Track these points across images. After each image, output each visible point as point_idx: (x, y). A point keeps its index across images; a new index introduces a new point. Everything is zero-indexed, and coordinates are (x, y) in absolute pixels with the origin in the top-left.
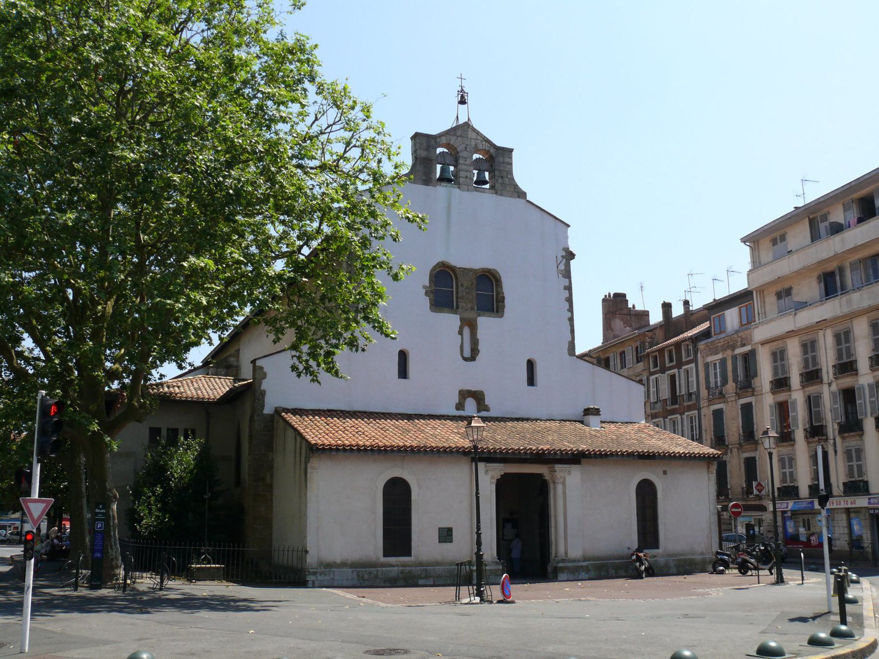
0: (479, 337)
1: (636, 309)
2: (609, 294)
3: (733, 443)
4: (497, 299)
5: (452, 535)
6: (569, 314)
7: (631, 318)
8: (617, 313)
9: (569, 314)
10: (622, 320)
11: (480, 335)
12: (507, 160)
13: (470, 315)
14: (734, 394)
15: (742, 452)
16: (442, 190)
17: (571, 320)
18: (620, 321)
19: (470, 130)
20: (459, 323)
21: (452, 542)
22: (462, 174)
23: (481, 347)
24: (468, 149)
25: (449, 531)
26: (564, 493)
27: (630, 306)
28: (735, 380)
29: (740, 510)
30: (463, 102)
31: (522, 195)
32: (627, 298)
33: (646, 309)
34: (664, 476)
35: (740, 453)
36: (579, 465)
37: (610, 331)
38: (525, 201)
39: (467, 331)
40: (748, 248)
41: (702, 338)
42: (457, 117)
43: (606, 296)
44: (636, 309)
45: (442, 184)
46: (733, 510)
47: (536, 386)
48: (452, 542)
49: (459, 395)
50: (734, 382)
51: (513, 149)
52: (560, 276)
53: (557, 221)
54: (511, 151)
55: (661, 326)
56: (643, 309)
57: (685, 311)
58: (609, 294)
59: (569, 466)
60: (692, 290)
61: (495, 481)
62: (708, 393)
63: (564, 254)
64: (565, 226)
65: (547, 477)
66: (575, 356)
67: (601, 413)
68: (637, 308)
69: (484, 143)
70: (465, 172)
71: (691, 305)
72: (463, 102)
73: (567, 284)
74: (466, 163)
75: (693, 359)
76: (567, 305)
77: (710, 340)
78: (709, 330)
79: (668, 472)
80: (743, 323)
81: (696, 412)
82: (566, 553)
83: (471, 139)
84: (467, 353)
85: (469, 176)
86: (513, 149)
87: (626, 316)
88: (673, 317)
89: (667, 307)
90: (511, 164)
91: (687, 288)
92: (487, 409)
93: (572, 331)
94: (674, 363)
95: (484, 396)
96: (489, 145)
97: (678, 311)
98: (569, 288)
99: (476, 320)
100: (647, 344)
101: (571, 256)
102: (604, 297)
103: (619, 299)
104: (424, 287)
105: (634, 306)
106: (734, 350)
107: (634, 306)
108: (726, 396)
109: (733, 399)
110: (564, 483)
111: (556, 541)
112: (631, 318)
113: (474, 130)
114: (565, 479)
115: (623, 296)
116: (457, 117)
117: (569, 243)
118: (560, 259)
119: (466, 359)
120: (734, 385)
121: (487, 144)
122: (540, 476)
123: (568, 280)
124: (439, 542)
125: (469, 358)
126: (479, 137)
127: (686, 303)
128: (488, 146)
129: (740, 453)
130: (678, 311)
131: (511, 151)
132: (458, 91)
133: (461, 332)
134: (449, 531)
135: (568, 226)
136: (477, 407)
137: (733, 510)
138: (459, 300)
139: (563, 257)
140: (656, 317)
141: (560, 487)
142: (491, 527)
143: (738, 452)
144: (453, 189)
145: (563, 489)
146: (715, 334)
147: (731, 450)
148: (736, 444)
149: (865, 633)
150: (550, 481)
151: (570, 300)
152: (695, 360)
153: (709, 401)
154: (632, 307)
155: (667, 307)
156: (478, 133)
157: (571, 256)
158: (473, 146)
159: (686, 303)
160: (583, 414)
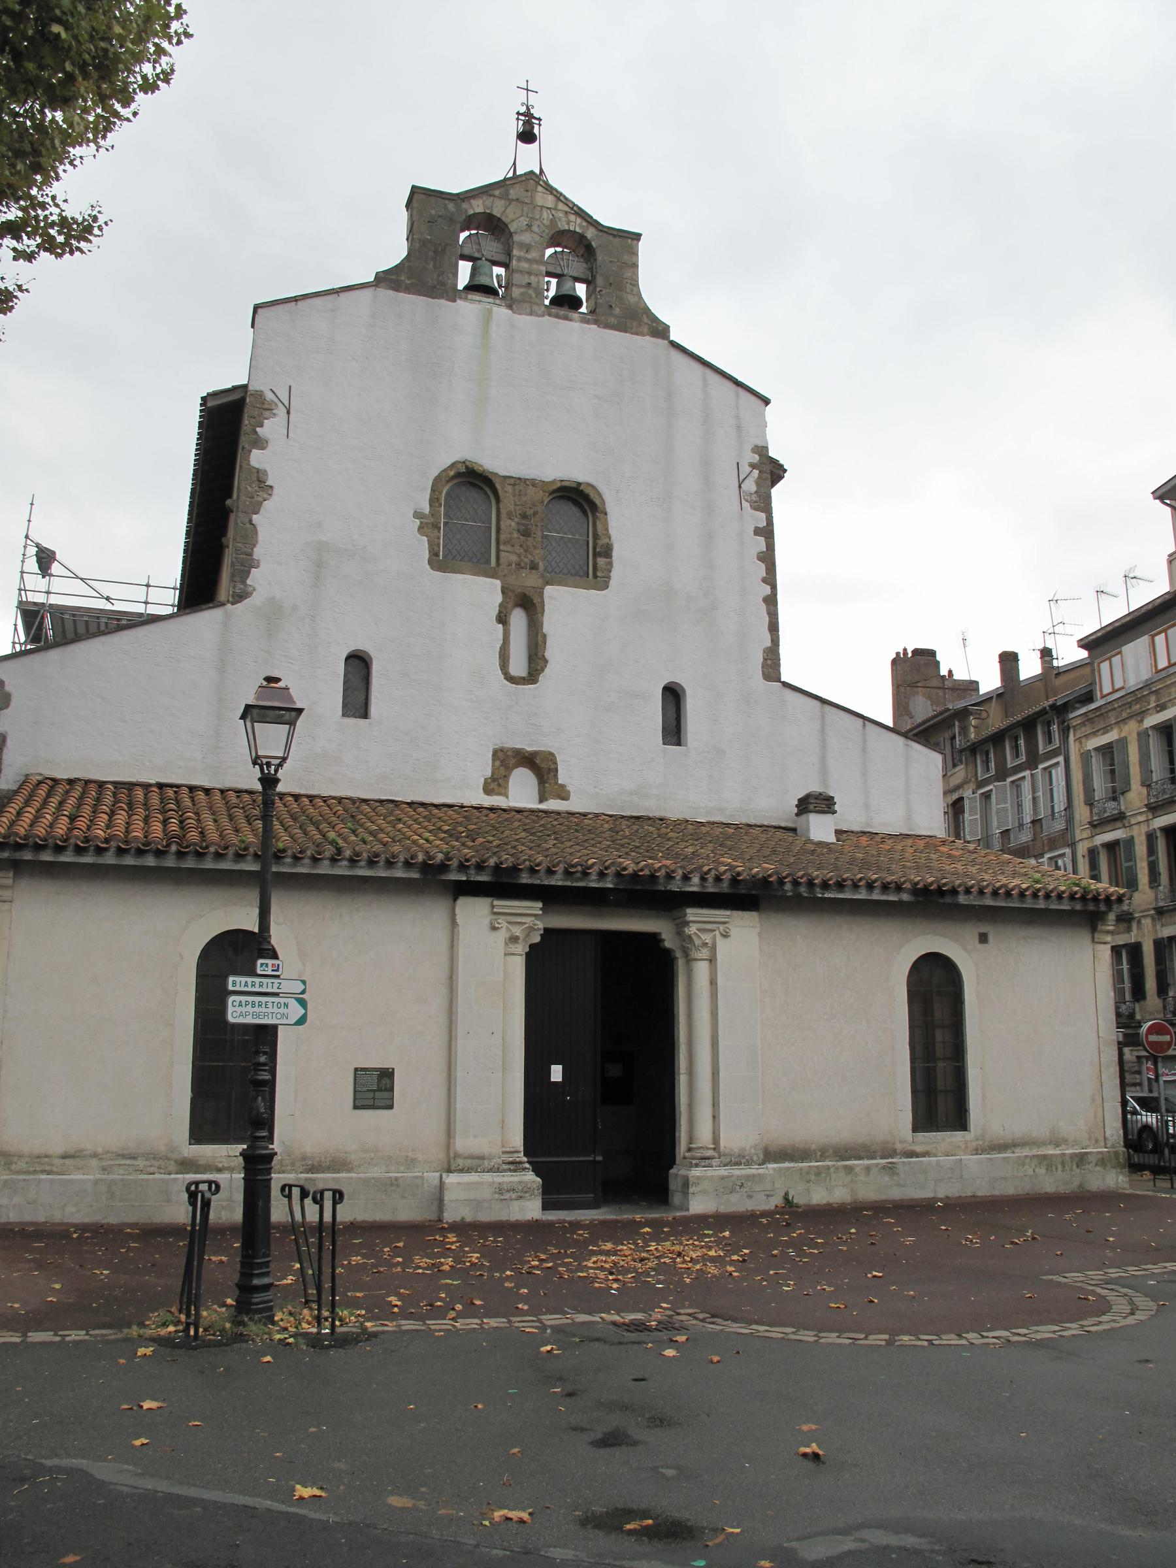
0: (546, 628)
1: (956, 677)
2: (905, 650)
3: (1143, 907)
4: (594, 548)
5: (391, 1089)
6: (767, 590)
7: (945, 694)
8: (919, 684)
9: (767, 590)
10: (929, 698)
11: (550, 623)
12: (634, 260)
13: (530, 580)
14: (1145, 809)
15: (1162, 925)
16: (470, 309)
17: (771, 601)
18: (924, 699)
19: (540, 189)
20: (499, 598)
21: (391, 1107)
22: (518, 278)
23: (552, 651)
24: (535, 228)
25: (386, 1075)
26: (713, 982)
27: (944, 672)
28: (1146, 783)
29: (1167, 1038)
30: (527, 136)
31: (660, 331)
32: (938, 658)
33: (973, 679)
34: (979, 946)
35: (1158, 927)
36: (755, 914)
37: (906, 717)
38: (666, 342)
39: (518, 618)
40: (1169, 509)
41: (1077, 705)
42: (514, 164)
43: (898, 654)
44: (956, 677)
45: (470, 296)
46: (1153, 1038)
47: (686, 745)
48: (391, 1107)
49: (494, 760)
50: (1143, 784)
51: (640, 235)
52: (746, 505)
53: (740, 390)
54: (637, 237)
55: (999, 696)
56: (969, 679)
57: (1043, 668)
58: (905, 650)
59: (728, 913)
60: (1057, 629)
61: (521, 948)
62: (1091, 812)
63: (756, 458)
64: (761, 404)
65: (669, 941)
66: (779, 680)
67: (836, 807)
68: (957, 676)
69: (572, 218)
70: (527, 276)
71: (1055, 657)
72: (527, 136)
73: (763, 523)
74: (529, 256)
75: (1059, 748)
76: (762, 569)
77: (1093, 706)
78: (1091, 691)
79: (991, 938)
80: (1160, 667)
81: (1068, 851)
82: (716, 1140)
83: (542, 207)
84: (519, 666)
85: (534, 285)
86: (640, 235)
87: (935, 690)
88: (1022, 678)
89: (1009, 661)
90: (635, 266)
91: (1047, 626)
92: (563, 794)
93: (774, 628)
94: (1023, 758)
95: (556, 763)
96: (584, 224)
97: (1029, 668)
98: (767, 532)
99: (541, 594)
100: (972, 729)
101: (773, 472)
102: (894, 656)
103: (922, 660)
104: (417, 515)
105: (950, 672)
106: (1141, 721)
107: (950, 672)
108: (1128, 814)
109: (1141, 818)
110: (712, 960)
111: (691, 1106)
112: (945, 694)
113: (550, 189)
114: (713, 948)
115: (931, 653)
116: (514, 164)
117: (769, 437)
118: (745, 469)
119: (511, 679)
120: (1144, 791)
121: (579, 220)
122: (653, 939)
123: (763, 515)
124: (356, 1107)
125: (523, 678)
126: (561, 206)
127: (1046, 653)
128: (580, 225)
129: (1158, 927)
130: (1029, 668)
131: (637, 237)
132: (518, 113)
133: (502, 619)
134: (386, 1075)
135: (766, 401)
136: (539, 790)
137: (1153, 1038)
138: (502, 547)
139: (753, 466)
140: (990, 681)
141: (701, 970)
142: (504, 1069)
143: (1154, 926)
144: (495, 309)
145: (711, 974)
146: (1103, 697)
147: (1139, 922)
148: (1148, 910)
149: (563, 783)
150: (678, 954)
151: (768, 559)
152: (1064, 750)
153: (1093, 825)
154: (947, 674)
155: (1009, 661)
156: (558, 196)
157: (773, 472)
158: (546, 222)
159: (1046, 653)
160: (795, 810)
